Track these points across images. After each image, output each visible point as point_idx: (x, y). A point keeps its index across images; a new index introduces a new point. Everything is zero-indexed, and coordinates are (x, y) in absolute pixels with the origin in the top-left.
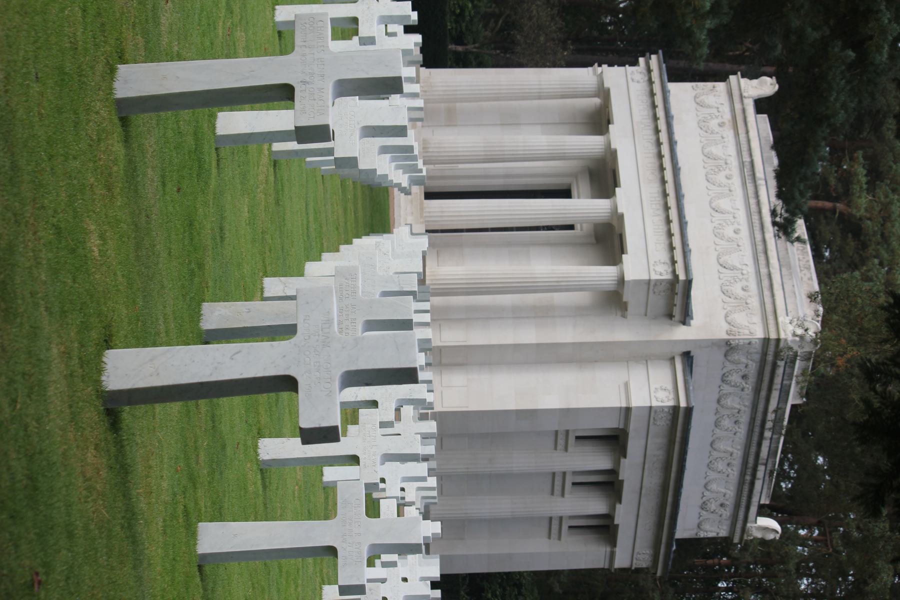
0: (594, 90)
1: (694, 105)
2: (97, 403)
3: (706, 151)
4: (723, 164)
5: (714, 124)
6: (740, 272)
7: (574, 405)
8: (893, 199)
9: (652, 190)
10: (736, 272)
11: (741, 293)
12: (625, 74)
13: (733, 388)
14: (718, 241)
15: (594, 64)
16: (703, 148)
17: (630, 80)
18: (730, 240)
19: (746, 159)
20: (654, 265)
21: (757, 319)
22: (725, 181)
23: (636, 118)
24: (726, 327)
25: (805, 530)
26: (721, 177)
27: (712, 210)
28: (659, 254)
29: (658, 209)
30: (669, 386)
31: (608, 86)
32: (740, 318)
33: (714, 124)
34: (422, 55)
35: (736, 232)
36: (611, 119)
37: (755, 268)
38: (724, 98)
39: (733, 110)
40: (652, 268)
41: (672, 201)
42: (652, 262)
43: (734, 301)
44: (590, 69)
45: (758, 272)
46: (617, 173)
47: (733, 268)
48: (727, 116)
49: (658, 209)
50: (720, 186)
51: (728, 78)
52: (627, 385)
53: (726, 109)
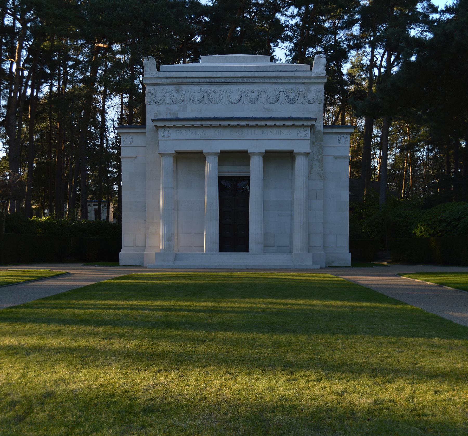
2: (50, 388)
3: (197, 102)
6: (281, 93)
7: (347, 184)
9: (250, 134)
10: (281, 95)
11: (255, 94)
12: (164, 141)
13: (314, 104)
14: (280, 102)
17: (169, 139)
18: (259, 95)
19: (205, 80)
20: (301, 137)
21: (312, 88)
22: (218, 95)
26: (216, 96)
27: (277, 103)
28: (294, 133)
29: (263, 131)
30: (337, 136)
32: (311, 96)
34: (350, 254)
35: (253, 91)
37: (279, 84)
38: (158, 89)
39: (168, 84)
40: (302, 138)
41: (198, 123)
42: (299, 138)
43: (300, 98)
44: (122, 160)
45: (282, 83)
47: (279, 96)
48: (172, 88)
49: (263, 131)
50: (222, 97)
52: (335, 157)
53: (167, 88)
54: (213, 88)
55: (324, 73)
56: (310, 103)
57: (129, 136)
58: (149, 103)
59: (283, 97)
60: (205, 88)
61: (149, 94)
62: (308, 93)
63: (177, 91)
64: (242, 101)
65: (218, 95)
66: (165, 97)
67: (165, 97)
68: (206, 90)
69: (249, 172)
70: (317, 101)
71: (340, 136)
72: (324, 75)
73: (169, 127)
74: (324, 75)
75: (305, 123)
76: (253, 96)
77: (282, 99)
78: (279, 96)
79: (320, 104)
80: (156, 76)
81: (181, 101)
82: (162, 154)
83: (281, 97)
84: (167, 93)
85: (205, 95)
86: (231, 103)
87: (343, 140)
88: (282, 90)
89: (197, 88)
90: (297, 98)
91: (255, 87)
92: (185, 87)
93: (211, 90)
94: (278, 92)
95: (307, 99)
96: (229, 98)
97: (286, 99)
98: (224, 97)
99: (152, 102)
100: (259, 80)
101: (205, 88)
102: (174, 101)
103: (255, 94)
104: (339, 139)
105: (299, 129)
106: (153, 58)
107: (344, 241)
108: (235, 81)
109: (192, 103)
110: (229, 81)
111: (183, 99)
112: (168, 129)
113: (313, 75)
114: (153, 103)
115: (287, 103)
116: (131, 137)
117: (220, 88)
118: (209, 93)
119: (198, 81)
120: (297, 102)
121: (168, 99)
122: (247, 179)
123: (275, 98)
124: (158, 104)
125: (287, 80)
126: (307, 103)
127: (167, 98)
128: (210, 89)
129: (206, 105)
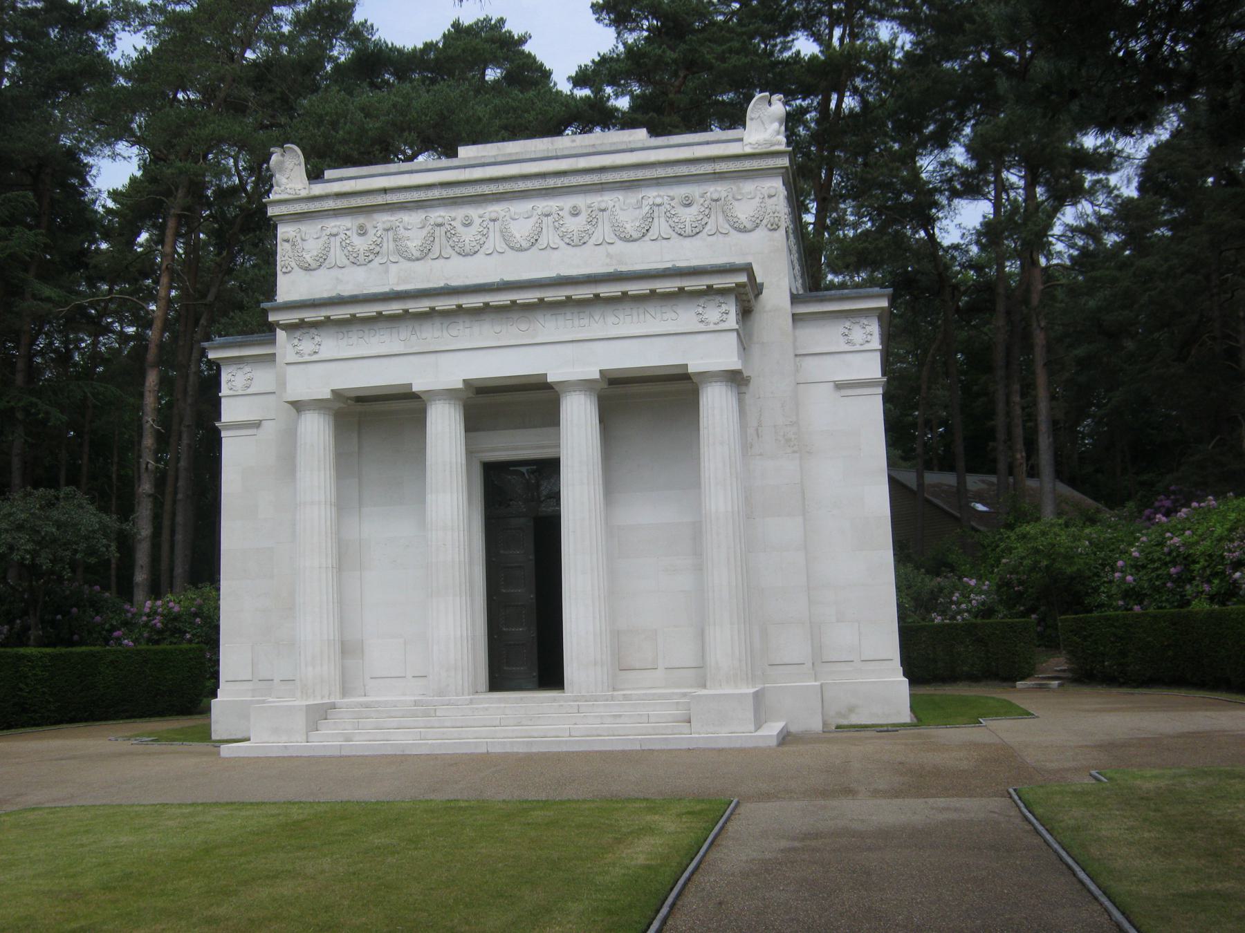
0: (322, 420)
1: (322, 271)
4: (443, 229)
5: (360, 244)
8: (1142, 48)
9: (550, 328)
10: (656, 214)
11: (582, 218)
14: (653, 233)
15: (217, 427)
16: (409, 259)
17: (315, 358)
20: (708, 324)
23: (670, 327)
24: (761, 233)
25: (141, 172)
26: (468, 236)
27: (646, 238)
28: (684, 317)
31: (329, 391)
32: (744, 212)
33: (360, 244)
35: (575, 213)
36: (353, 394)
37: (648, 186)
38: (310, 230)
40: (712, 327)
42: (702, 327)
43: (713, 217)
44: (223, 434)
45: (658, 182)
46: (533, 381)
47: (650, 217)
51: (270, 218)
52: (839, 386)
53: (333, 225)
54: (460, 213)
55: (781, 142)
56: (743, 230)
57: (241, 366)
58: (284, 270)
59: (663, 220)
60: (437, 214)
61: (286, 244)
62: (736, 204)
63: (362, 232)
64: (543, 242)
65: (474, 229)
66: (327, 248)
67: (327, 248)
68: (440, 220)
69: (559, 446)
70: (765, 222)
71: (848, 324)
72: (783, 147)
73: (315, 325)
74: (783, 147)
75: (718, 282)
76: (574, 225)
77: (661, 226)
78: (650, 217)
79: (775, 230)
80: (304, 193)
81: (372, 257)
82: (298, 406)
83: (656, 220)
84: (332, 239)
85: (437, 234)
86: (512, 248)
87: (858, 334)
88: (658, 201)
89: (412, 219)
90: (706, 219)
91: (581, 201)
92: (383, 219)
93: (454, 219)
94: (648, 207)
95: (735, 220)
96: (506, 237)
97: (673, 225)
98: (491, 234)
99: (293, 264)
100: (588, 179)
101: (438, 215)
102: (352, 259)
103: (582, 218)
104: (847, 332)
105: (702, 301)
106: (300, 152)
107: (887, 643)
108: (522, 186)
109: (401, 260)
110: (501, 188)
111: (378, 249)
112: (313, 331)
113: (748, 150)
114: (296, 268)
115: (674, 235)
116: (247, 369)
117: (481, 211)
118: (449, 227)
119: (415, 196)
120: (706, 230)
121: (337, 255)
122: (549, 468)
123: (638, 224)
124: (307, 269)
125: (670, 172)
126: (735, 232)
127: (332, 250)
128: (453, 214)
129: (442, 261)
